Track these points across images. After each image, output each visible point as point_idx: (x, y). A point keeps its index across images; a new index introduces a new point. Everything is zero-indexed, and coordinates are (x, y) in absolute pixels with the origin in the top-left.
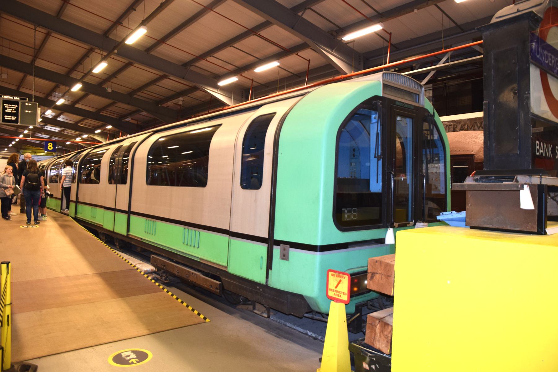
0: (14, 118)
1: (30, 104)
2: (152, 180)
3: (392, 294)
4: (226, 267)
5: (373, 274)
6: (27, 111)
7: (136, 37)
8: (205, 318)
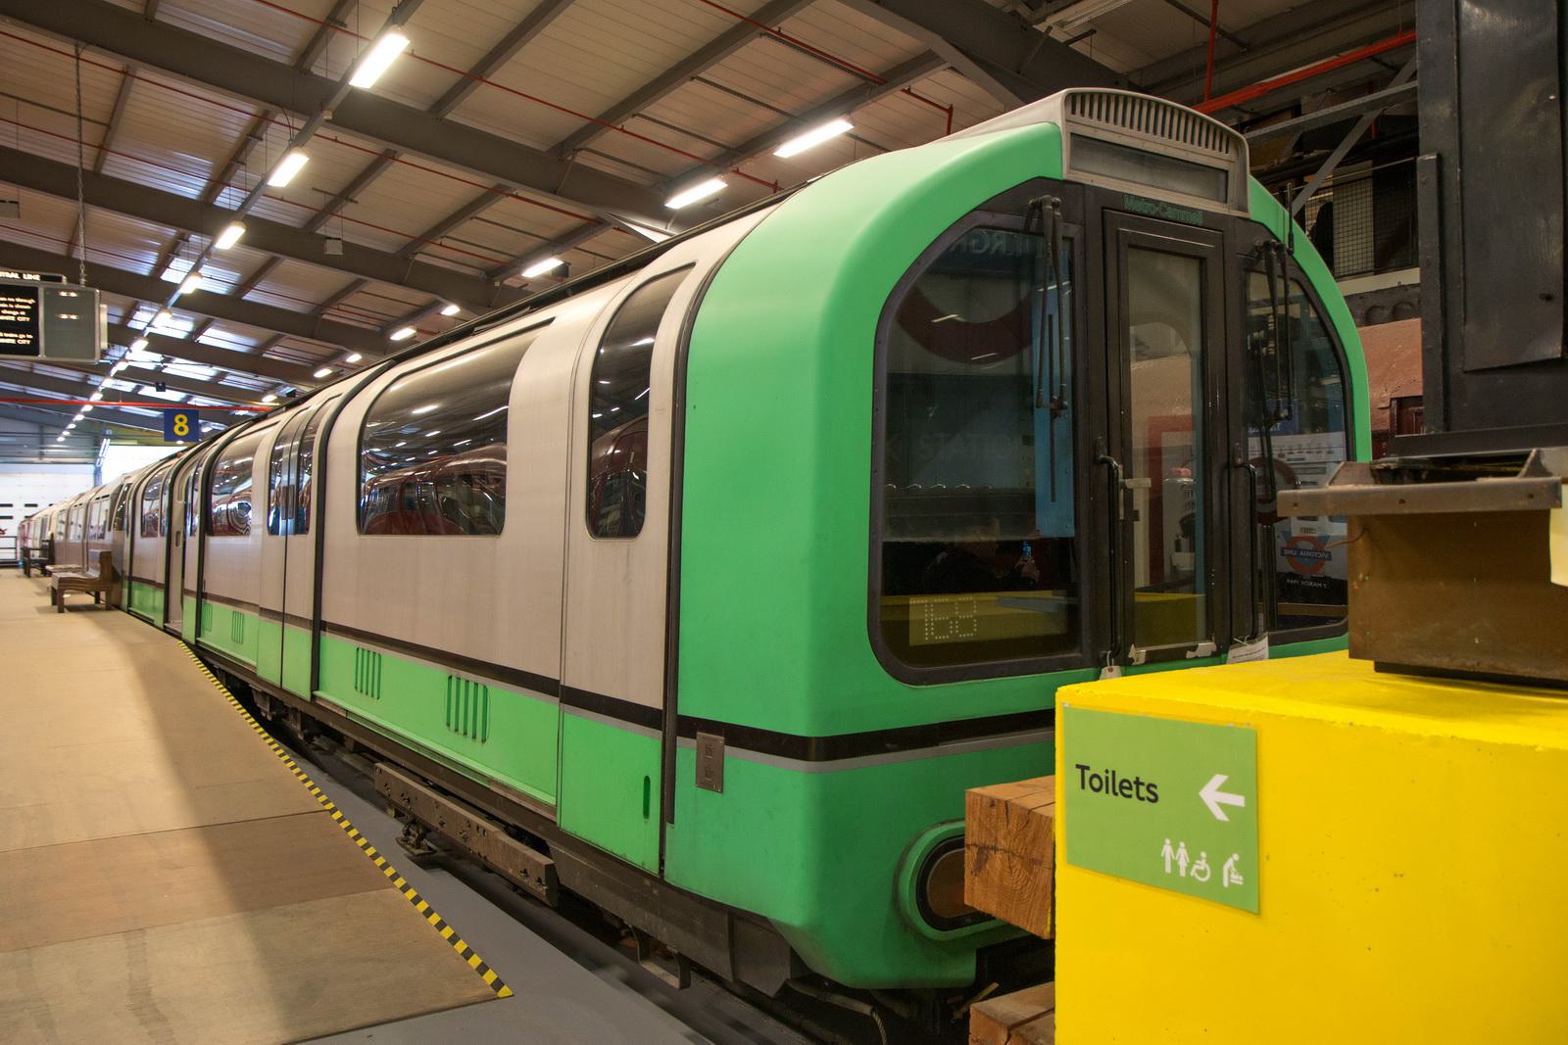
0: (24, 340)
1: (73, 295)
2: (369, 522)
3: (1046, 936)
4: (553, 809)
5: (984, 851)
6: (64, 317)
7: (379, 61)
8: (498, 984)
